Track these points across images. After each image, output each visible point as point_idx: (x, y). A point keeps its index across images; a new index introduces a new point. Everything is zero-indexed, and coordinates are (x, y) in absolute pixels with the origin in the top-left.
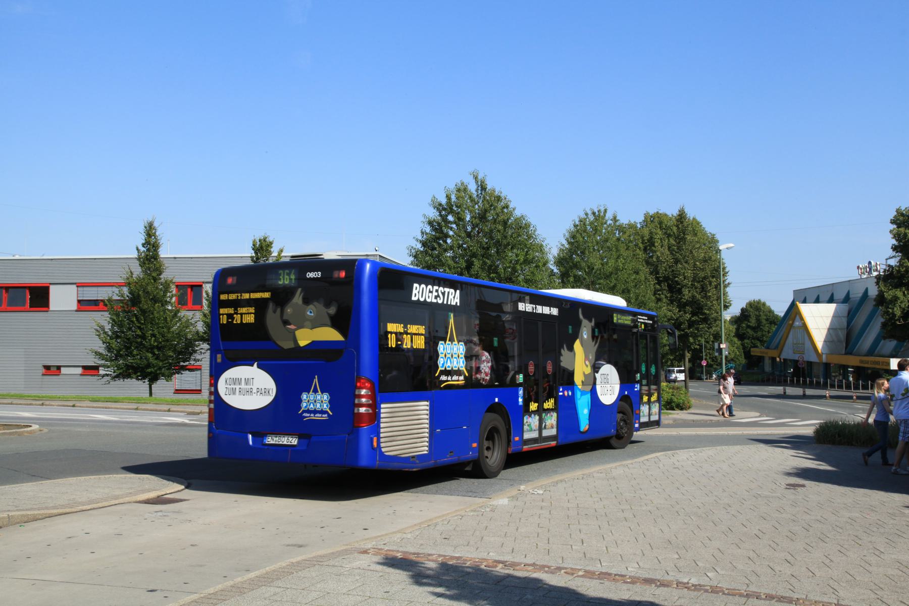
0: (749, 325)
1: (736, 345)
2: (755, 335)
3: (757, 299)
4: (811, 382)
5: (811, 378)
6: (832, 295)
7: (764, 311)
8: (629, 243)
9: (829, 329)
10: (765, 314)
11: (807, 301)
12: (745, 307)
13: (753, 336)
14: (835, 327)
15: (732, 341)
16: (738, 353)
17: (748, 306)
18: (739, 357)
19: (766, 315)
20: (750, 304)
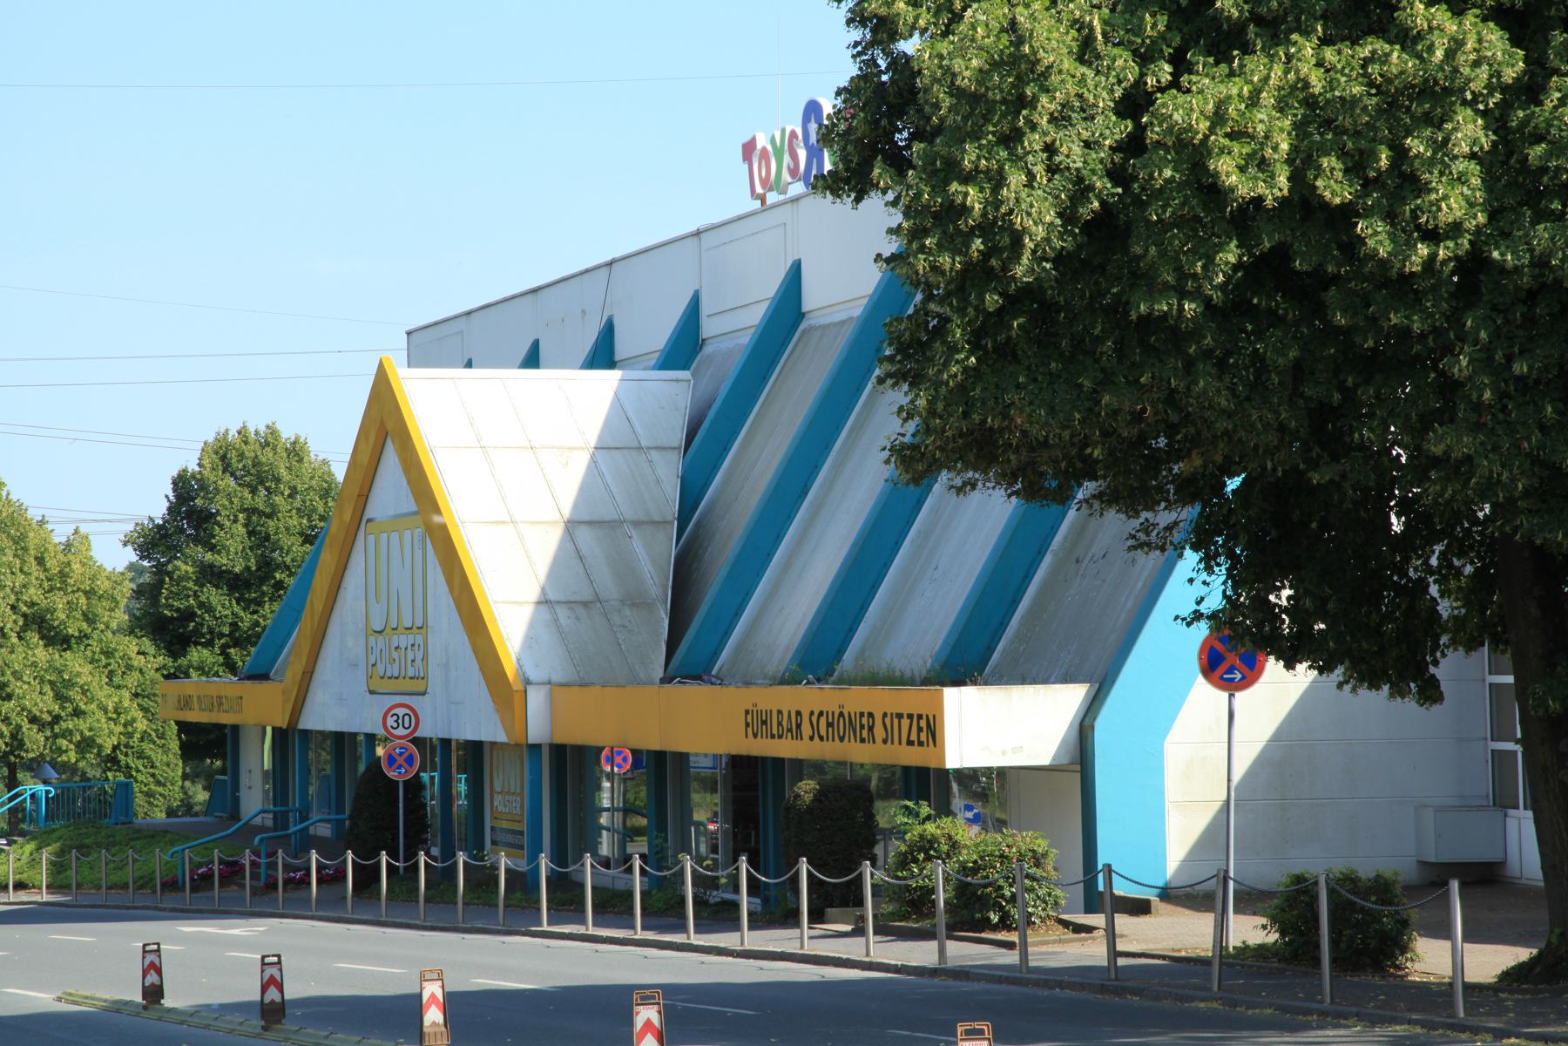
0: (211, 566)
1: (133, 679)
2: (247, 620)
3: (257, 424)
4: (482, 880)
5: (476, 845)
6: (608, 332)
7: (294, 492)
8: (267, 489)
9: (572, 526)
10: (297, 503)
11: (473, 365)
12: (193, 467)
13: (234, 625)
14: (608, 513)
15: (108, 654)
16: (142, 725)
17: (206, 462)
18: (147, 747)
19: (305, 512)
20: (223, 455)
